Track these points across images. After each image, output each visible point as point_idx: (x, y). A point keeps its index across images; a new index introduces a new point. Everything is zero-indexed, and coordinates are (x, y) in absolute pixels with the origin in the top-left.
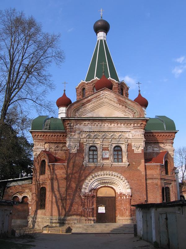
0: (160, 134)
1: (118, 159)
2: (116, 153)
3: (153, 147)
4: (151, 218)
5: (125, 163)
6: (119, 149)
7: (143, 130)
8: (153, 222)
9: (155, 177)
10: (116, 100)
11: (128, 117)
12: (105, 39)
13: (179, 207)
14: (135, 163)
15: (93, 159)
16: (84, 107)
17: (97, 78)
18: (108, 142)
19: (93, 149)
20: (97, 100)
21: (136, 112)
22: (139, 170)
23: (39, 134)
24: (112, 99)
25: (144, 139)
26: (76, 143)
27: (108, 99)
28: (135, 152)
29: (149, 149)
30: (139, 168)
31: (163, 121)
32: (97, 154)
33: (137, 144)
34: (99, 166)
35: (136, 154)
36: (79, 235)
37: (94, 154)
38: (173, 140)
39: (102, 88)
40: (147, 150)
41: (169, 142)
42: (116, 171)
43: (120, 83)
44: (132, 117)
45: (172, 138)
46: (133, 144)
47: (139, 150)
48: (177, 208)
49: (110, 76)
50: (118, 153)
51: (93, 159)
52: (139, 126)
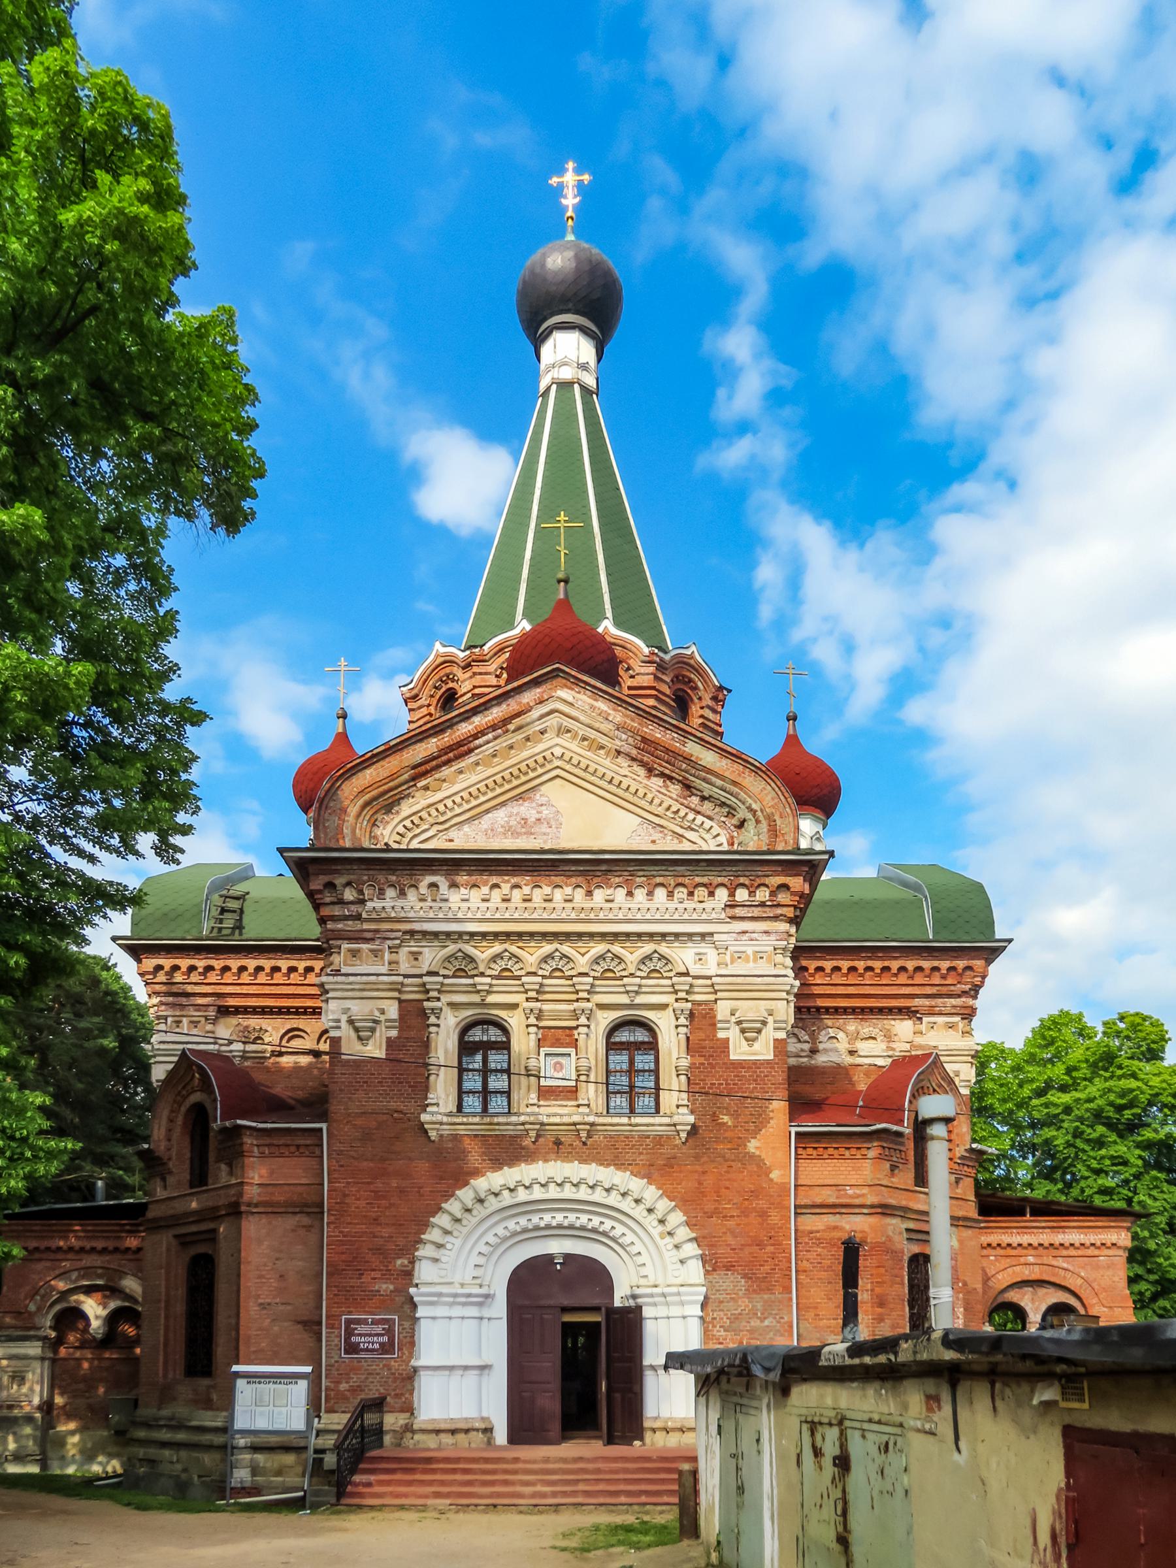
0: (896, 958)
1: (631, 1092)
2: (620, 1060)
5: (676, 1119)
6: (641, 1036)
7: (784, 926)
9: (851, 1197)
10: (623, 742)
11: (695, 848)
12: (590, 381)
13: (930, 1385)
14: (735, 1115)
15: (485, 1093)
16: (426, 788)
18: (574, 997)
20: (511, 747)
21: (749, 816)
22: (752, 1157)
23: (177, 962)
25: (791, 980)
26: (384, 1004)
27: (574, 737)
28: (732, 1057)
30: (753, 1146)
31: (916, 888)
32: (505, 1066)
33: (751, 1010)
34: (517, 1136)
35: (740, 1064)
38: (975, 997)
39: (532, 670)
40: (814, 1051)
41: (948, 1010)
42: (618, 1163)
43: (667, 657)
44: (725, 847)
45: (967, 987)
46: (723, 1010)
47: (757, 1046)
48: (914, 1397)
49: (609, 614)
50: (632, 1062)
51: (485, 1093)
52: (763, 904)
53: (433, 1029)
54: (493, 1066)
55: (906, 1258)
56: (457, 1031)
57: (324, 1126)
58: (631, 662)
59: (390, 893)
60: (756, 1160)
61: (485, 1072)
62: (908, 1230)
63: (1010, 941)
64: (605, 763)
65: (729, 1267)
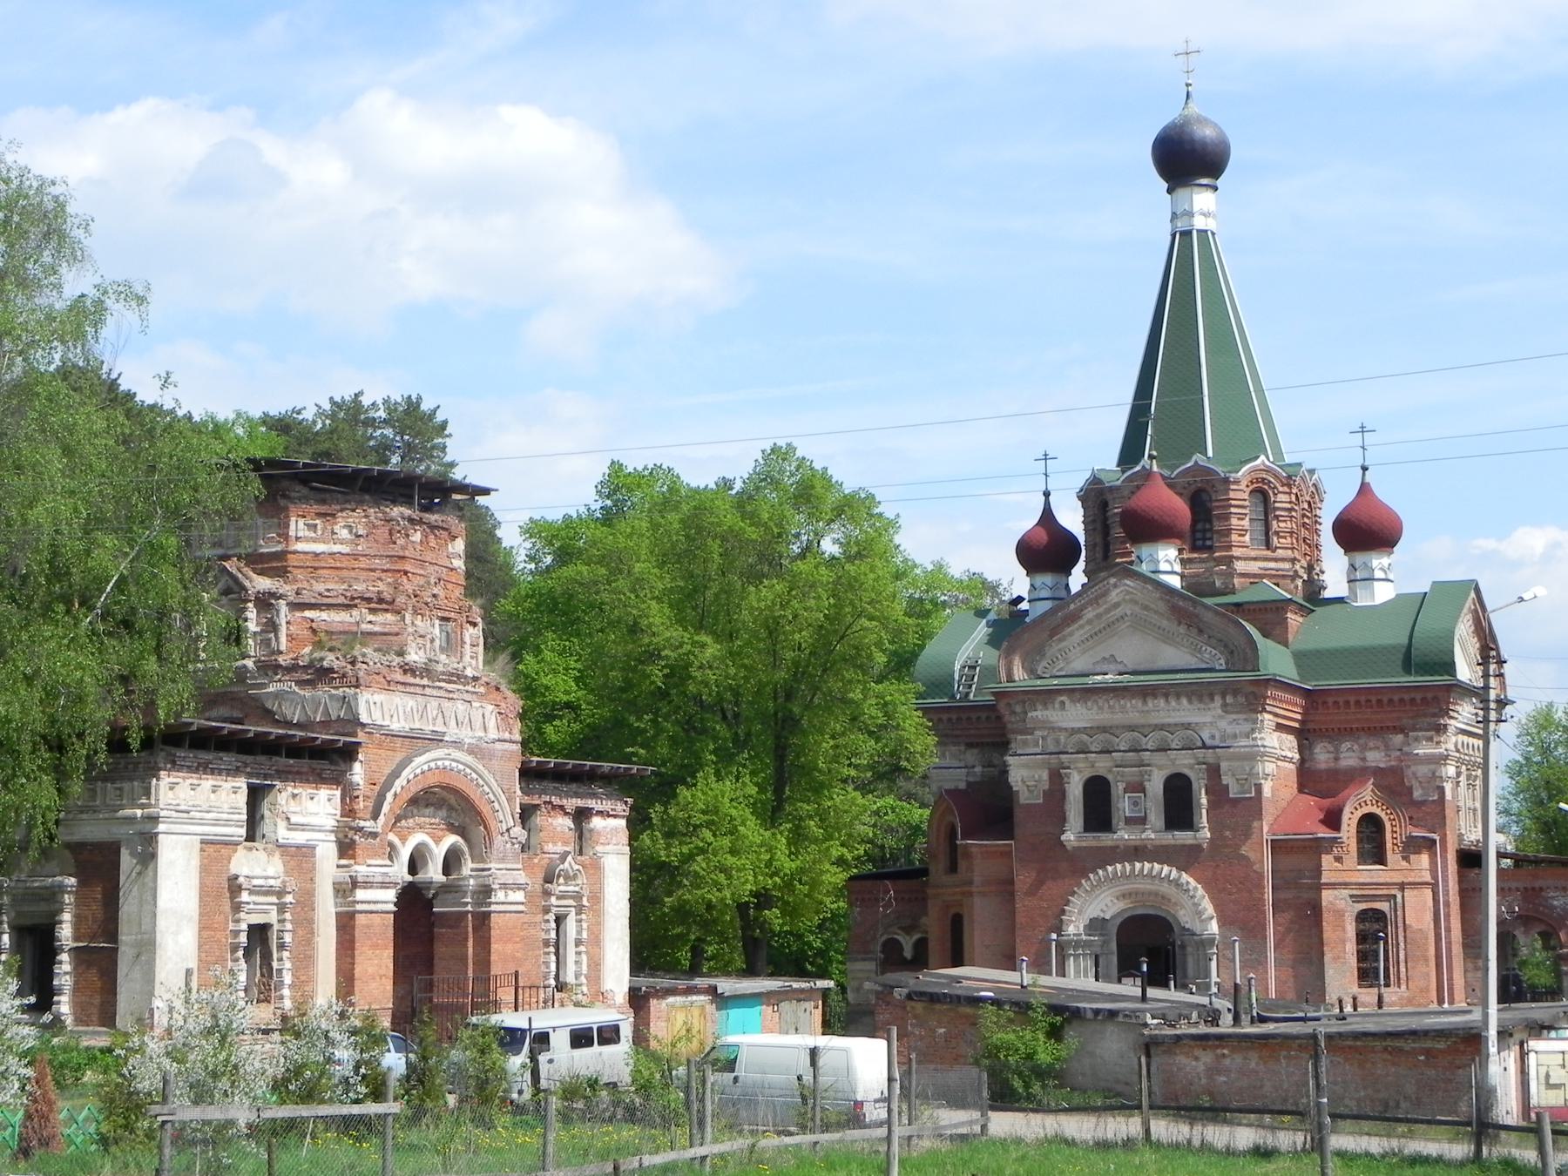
3: (1364, 748)
24: (1153, 606)
28: (1231, 796)
29: (1348, 754)
57: (1012, 842)
60: (1246, 858)
62: (1351, 896)
64: (1155, 618)
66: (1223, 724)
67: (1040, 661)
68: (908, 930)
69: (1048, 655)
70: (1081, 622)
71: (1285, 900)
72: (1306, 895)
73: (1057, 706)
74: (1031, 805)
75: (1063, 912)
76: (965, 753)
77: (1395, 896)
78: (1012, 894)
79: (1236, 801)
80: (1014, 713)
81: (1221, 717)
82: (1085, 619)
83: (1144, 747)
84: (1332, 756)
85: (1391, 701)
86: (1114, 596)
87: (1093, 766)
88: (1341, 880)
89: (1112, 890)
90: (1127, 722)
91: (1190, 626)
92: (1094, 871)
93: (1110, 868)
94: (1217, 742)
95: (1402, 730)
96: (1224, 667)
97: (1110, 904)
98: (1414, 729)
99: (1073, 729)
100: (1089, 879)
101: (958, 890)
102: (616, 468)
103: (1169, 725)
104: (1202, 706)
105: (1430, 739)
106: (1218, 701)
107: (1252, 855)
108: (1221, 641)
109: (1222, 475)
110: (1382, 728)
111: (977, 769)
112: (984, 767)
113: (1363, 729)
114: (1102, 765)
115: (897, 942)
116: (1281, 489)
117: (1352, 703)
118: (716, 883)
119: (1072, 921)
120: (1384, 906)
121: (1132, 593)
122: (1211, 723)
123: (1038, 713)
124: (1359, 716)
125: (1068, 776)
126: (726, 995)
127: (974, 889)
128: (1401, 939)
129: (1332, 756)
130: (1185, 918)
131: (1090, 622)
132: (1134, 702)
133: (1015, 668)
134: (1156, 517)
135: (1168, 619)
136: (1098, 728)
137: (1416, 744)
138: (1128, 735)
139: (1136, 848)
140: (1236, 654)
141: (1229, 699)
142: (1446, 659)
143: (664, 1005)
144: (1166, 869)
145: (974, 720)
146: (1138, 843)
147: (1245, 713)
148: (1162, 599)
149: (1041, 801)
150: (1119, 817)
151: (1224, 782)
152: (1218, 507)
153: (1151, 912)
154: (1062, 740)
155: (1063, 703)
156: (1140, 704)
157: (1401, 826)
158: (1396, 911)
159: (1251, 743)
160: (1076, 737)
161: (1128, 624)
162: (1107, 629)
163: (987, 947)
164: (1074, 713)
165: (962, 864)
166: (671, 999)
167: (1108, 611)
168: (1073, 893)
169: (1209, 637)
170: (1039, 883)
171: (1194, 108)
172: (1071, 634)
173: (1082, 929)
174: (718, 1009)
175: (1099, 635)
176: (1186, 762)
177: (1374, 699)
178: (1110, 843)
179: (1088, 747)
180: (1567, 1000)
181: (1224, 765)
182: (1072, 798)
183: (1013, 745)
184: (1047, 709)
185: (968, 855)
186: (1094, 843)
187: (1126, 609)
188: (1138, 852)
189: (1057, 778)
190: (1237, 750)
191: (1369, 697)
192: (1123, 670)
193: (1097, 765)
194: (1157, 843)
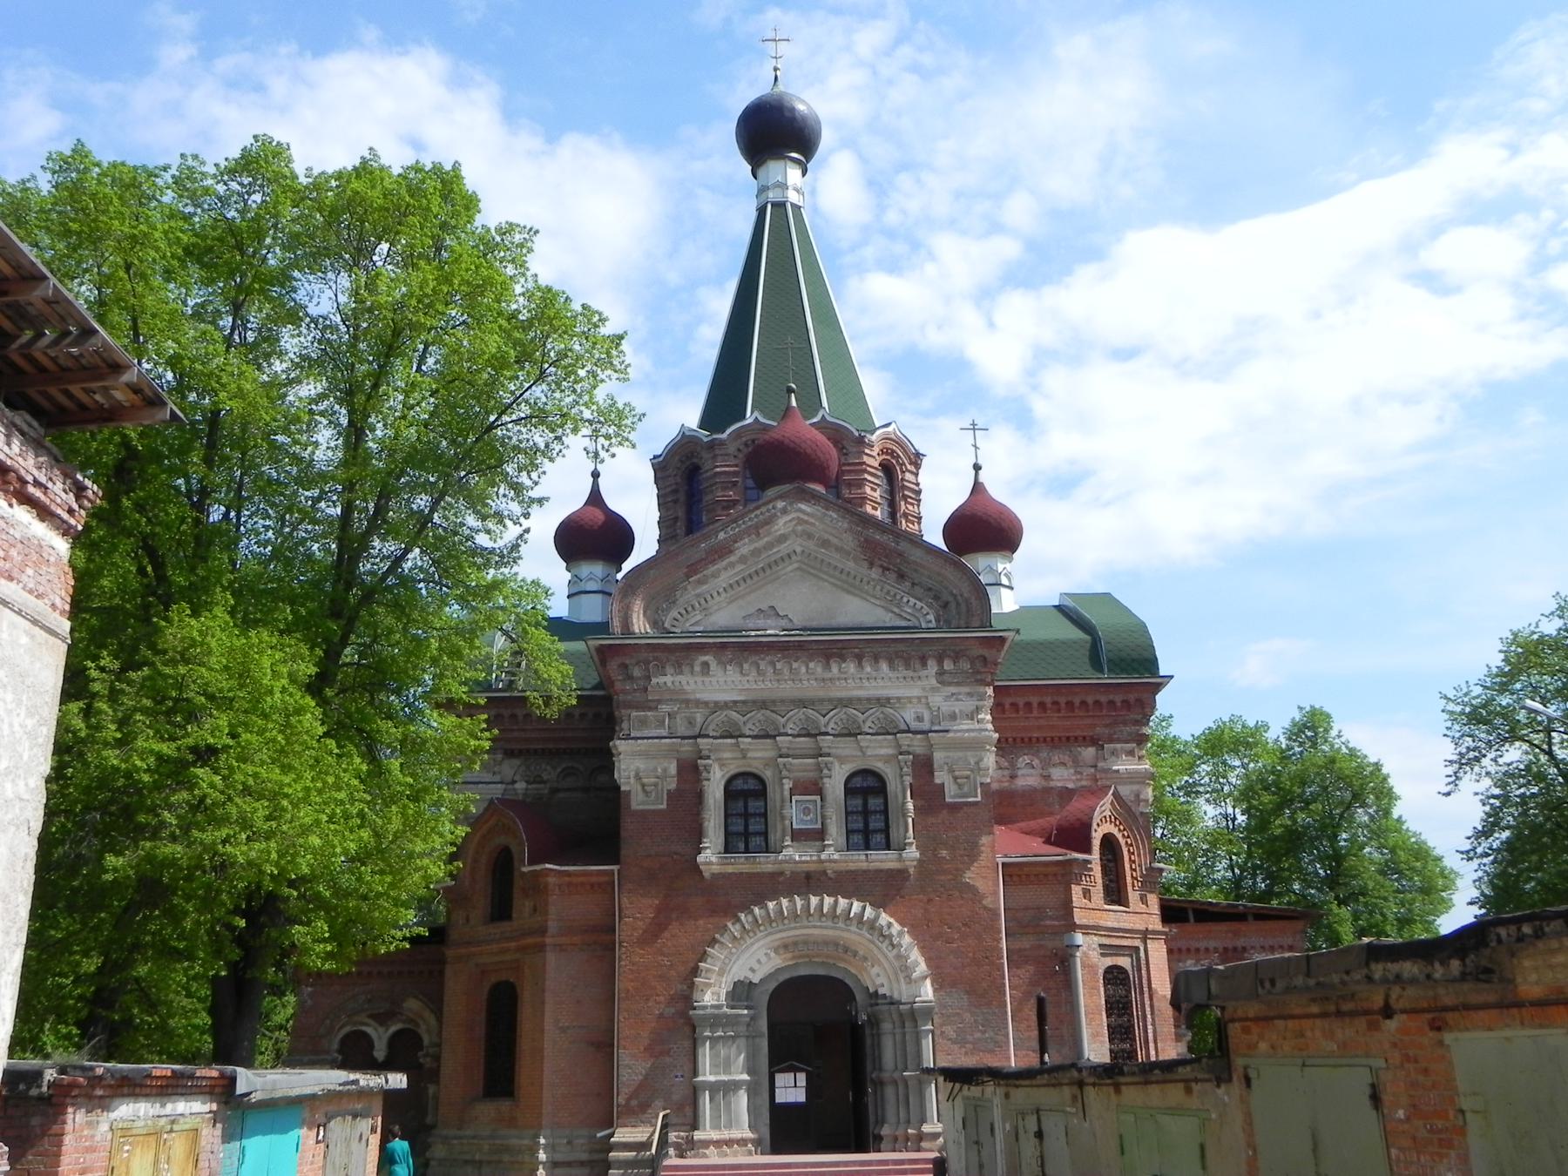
2: (857, 802)
3: (1047, 764)
4: (992, 1130)
8: (998, 1148)
11: (910, 624)
17: (756, 414)
19: (746, 787)
24: (834, 541)
28: (948, 800)
36: (1481, 1013)
37: (751, 810)
40: (1013, 777)
50: (865, 804)
53: (705, 783)
54: (751, 810)
55: (1101, 972)
56: (723, 783)
57: (615, 868)
58: (845, 442)
59: (669, 669)
60: (972, 889)
61: (746, 816)
62: (1101, 946)
63: (1172, 677)
64: (835, 558)
65: (954, 984)
66: (937, 700)
67: (668, 610)
68: (382, 1019)
69: (681, 600)
70: (733, 558)
71: (1020, 950)
72: (1051, 944)
73: (697, 668)
74: (648, 811)
75: (695, 971)
76: (500, 763)
77: (1137, 949)
78: (611, 948)
79: (955, 807)
80: (630, 678)
81: (933, 689)
82: (738, 554)
83: (823, 730)
84: (1006, 772)
85: (1083, 703)
86: (782, 525)
87: (744, 757)
88: (1091, 923)
89: (769, 939)
90: (797, 694)
91: (885, 569)
92: (746, 908)
93: (771, 905)
94: (926, 726)
95: (1094, 741)
96: (933, 625)
97: (764, 959)
98: (1111, 741)
99: (716, 703)
100: (739, 920)
101: (513, 944)
102: (80, 151)
103: (859, 699)
104: (910, 673)
105: (1131, 753)
106: (932, 667)
107: (980, 885)
108: (930, 589)
109: (857, 434)
110: (1068, 738)
111: (517, 786)
112: (527, 782)
113: (1045, 740)
114: (758, 756)
115: (365, 1034)
116: (909, 467)
117: (1035, 705)
118: (245, 823)
119: (709, 985)
120: (1125, 962)
121: (806, 522)
122: (919, 698)
123: (668, 679)
124: (1042, 722)
125: (707, 769)
126: (255, 1097)
127: (548, 940)
128: (1148, 1009)
129: (1006, 772)
130: (877, 978)
131: (743, 559)
132: (812, 665)
133: (635, 616)
134: (809, 451)
135: (855, 559)
136: (754, 702)
137: (1114, 758)
138: (799, 714)
139: (808, 876)
140: (953, 606)
141: (948, 665)
142: (1146, 655)
143: (104, 1127)
144: (856, 906)
145: (521, 718)
146: (812, 867)
147: (968, 685)
148: (851, 530)
149: (664, 806)
150: (784, 830)
151: (938, 781)
152: (850, 472)
153: (821, 972)
154: (699, 719)
155: (706, 665)
156: (819, 670)
157: (1139, 855)
158: (1139, 970)
159: (977, 726)
160: (721, 716)
161: (796, 565)
162: (765, 572)
163: (563, 1030)
164: (722, 680)
165: (522, 907)
166: (127, 1110)
167: (770, 546)
168: (713, 942)
169: (913, 584)
170: (656, 930)
171: (781, 87)
172: (715, 575)
173: (723, 997)
174: (227, 1138)
175: (755, 578)
176: (883, 751)
177: (1062, 700)
178: (769, 868)
179: (739, 730)
180: (6, 1174)
181: (938, 756)
182: (711, 802)
183: (625, 725)
184: (681, 673)
185: (537, 886)
186: (745, 868)
187: (796, 545)
188: (810, 882)
189: (691, 772)
190: (959, 734)
191: (1056, 699)
192: (789, 626)
193: (749, 755)
194: (842, 867)
